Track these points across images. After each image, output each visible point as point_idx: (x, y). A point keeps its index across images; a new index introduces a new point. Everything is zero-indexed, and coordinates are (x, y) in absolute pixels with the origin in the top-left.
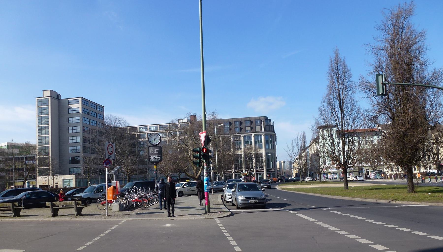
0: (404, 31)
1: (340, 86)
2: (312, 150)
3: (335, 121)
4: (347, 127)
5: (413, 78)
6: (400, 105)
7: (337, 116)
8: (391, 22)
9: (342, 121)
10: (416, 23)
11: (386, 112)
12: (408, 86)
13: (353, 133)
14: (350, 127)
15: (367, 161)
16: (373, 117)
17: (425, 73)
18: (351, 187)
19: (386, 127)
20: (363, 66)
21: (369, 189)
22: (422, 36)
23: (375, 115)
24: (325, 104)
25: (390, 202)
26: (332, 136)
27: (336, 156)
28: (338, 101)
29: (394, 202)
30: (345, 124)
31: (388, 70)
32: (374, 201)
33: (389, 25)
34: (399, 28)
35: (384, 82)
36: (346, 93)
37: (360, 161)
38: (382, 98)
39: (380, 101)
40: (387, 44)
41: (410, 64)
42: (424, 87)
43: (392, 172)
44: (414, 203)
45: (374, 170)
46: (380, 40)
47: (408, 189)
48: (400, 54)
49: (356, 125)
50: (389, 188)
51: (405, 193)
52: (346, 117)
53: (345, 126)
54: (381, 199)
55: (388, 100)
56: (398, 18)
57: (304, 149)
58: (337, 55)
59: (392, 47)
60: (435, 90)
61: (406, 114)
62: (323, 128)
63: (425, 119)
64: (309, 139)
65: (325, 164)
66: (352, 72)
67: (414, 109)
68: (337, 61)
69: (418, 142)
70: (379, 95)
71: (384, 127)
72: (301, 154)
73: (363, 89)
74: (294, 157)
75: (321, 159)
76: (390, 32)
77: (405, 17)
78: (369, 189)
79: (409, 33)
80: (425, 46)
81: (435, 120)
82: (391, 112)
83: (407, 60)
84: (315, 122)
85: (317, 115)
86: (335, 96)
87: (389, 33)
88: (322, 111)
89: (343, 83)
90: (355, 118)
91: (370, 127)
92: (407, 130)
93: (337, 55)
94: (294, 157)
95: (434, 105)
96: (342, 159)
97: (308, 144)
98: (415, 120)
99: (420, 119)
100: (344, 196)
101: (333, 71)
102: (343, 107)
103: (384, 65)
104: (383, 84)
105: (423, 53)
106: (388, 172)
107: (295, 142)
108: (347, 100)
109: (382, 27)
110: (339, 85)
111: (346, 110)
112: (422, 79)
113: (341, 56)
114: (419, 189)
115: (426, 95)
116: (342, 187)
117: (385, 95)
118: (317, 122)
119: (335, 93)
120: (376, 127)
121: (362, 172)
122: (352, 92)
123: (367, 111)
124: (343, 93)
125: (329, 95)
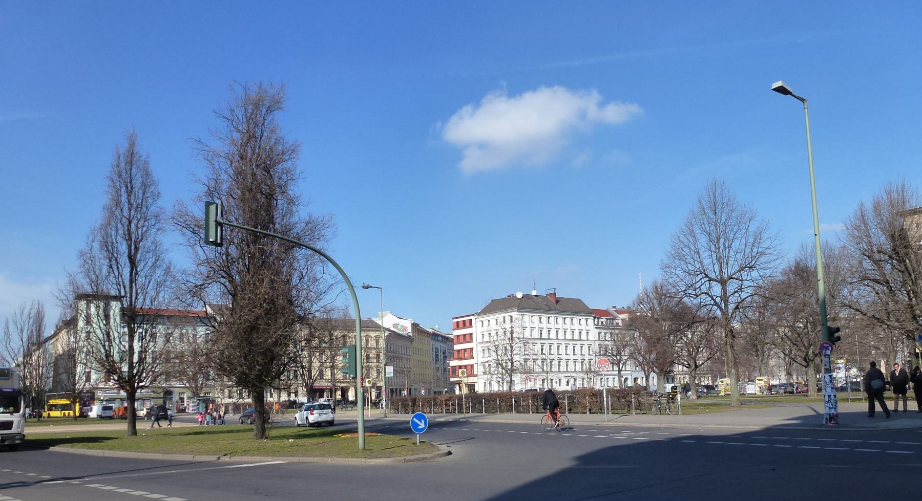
0: (265, 134)
1: (133, 212)
2: (60, 345)
3: (115, 286)
4: (140, 301)
5: (274, 225)
6: (248, 269)
7: (120, 275)
8: (243, 109)
9: (131, 288)
10: (286, 126)
11: (223, 280)
12: (266, 236)
13: (154, 317)
14: (148, 302)
15: (181, 375)
16: (196, 286)
17: (295, 219)
18: (143, 430)
19: (219, 309)
20: (187, 179)
21: (181, 435)
22: (293, 151)
23: (201, 282)
24: (96, 245)
25: (219, 458)
26: (107, 317)
27: (113, 361)
28: (125, 243)
29: (227, 459)
30: (137, 294)
31: (231, 200)
32: (188, 458)
33: (240, 113)
34: (256, 125)
35: (220, 220)
36: (145, 229)
37: (168, 376)
38: (217, 251)
39: (211, 255)
40: (234, 150)
41: (270, 197)
42: (291, 244)
43: (230, 401)
44: (262, 458)
45: (195, 394)
46: (224, 142)
47: (254, 433)
48: (254, 175)
49: (161, 299)
50: (221, 432)
51: (249, 440)
52: (141, 280)
53: (136, 298)
54: (202, 453)
55: (227, 258)
56: (257, 106)
57: (38, 342)
58: (132, 145)
59: (242, 158)
60: (309, 252)
61: (257, 288)
62: (88, 298)
63: (291, 302)
64: (53, 317)
65: (88, 379)
66: (161, 188)
67: (272, 281)
68: (131, 157)
69: (276, 344)
70: (207, 242)
71: (217, 309)
72: (28, 354)
73: (179, 227)
74: (10, 360)
75: (79, 369)
76: (241, 128)
77: (269, 110)
78: (181, 435)
79: (273, 141)
80: (298, 171)
81: (306, 305)
82: (232, 281)
83: (265, 189)
84: (67, 281)
85: (75, 266)
86: (121, 232)
87: (238, 131)
88: (86, 258)
89: (139, 207)
90: (159, 285)
91: (189, 305)
92: (257, 318)
93: (132, 145)
94: (10, 360)
95: (306, 279)
96: (125, 368)
97: (48, 331)
98: (272, 302)
99: (281, 301)
100: (126, 450)
101: (120, 176)
102: (135, 257)
103: (225, 187)
104: (218, 224)
105: (293, 182)
106: (223, 399)
107: (16, 323)
108: (146, 244)
109: (228, 114)
110: (130, 209)
111: (142, 264)
112: (288, 229)
113: (142, 149)
114: (274, 433)
115: (294, 258)
116: (124, 431)
117: (220, 245)
118: (72, 283)
119: (120, 226)
120: (198, 308)
121: (171, 399)
122: (158, 229)
123: (184, 272)
124: (137, 228)
125: (106, 226)
